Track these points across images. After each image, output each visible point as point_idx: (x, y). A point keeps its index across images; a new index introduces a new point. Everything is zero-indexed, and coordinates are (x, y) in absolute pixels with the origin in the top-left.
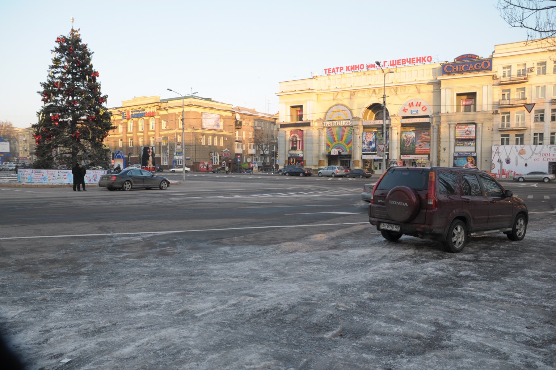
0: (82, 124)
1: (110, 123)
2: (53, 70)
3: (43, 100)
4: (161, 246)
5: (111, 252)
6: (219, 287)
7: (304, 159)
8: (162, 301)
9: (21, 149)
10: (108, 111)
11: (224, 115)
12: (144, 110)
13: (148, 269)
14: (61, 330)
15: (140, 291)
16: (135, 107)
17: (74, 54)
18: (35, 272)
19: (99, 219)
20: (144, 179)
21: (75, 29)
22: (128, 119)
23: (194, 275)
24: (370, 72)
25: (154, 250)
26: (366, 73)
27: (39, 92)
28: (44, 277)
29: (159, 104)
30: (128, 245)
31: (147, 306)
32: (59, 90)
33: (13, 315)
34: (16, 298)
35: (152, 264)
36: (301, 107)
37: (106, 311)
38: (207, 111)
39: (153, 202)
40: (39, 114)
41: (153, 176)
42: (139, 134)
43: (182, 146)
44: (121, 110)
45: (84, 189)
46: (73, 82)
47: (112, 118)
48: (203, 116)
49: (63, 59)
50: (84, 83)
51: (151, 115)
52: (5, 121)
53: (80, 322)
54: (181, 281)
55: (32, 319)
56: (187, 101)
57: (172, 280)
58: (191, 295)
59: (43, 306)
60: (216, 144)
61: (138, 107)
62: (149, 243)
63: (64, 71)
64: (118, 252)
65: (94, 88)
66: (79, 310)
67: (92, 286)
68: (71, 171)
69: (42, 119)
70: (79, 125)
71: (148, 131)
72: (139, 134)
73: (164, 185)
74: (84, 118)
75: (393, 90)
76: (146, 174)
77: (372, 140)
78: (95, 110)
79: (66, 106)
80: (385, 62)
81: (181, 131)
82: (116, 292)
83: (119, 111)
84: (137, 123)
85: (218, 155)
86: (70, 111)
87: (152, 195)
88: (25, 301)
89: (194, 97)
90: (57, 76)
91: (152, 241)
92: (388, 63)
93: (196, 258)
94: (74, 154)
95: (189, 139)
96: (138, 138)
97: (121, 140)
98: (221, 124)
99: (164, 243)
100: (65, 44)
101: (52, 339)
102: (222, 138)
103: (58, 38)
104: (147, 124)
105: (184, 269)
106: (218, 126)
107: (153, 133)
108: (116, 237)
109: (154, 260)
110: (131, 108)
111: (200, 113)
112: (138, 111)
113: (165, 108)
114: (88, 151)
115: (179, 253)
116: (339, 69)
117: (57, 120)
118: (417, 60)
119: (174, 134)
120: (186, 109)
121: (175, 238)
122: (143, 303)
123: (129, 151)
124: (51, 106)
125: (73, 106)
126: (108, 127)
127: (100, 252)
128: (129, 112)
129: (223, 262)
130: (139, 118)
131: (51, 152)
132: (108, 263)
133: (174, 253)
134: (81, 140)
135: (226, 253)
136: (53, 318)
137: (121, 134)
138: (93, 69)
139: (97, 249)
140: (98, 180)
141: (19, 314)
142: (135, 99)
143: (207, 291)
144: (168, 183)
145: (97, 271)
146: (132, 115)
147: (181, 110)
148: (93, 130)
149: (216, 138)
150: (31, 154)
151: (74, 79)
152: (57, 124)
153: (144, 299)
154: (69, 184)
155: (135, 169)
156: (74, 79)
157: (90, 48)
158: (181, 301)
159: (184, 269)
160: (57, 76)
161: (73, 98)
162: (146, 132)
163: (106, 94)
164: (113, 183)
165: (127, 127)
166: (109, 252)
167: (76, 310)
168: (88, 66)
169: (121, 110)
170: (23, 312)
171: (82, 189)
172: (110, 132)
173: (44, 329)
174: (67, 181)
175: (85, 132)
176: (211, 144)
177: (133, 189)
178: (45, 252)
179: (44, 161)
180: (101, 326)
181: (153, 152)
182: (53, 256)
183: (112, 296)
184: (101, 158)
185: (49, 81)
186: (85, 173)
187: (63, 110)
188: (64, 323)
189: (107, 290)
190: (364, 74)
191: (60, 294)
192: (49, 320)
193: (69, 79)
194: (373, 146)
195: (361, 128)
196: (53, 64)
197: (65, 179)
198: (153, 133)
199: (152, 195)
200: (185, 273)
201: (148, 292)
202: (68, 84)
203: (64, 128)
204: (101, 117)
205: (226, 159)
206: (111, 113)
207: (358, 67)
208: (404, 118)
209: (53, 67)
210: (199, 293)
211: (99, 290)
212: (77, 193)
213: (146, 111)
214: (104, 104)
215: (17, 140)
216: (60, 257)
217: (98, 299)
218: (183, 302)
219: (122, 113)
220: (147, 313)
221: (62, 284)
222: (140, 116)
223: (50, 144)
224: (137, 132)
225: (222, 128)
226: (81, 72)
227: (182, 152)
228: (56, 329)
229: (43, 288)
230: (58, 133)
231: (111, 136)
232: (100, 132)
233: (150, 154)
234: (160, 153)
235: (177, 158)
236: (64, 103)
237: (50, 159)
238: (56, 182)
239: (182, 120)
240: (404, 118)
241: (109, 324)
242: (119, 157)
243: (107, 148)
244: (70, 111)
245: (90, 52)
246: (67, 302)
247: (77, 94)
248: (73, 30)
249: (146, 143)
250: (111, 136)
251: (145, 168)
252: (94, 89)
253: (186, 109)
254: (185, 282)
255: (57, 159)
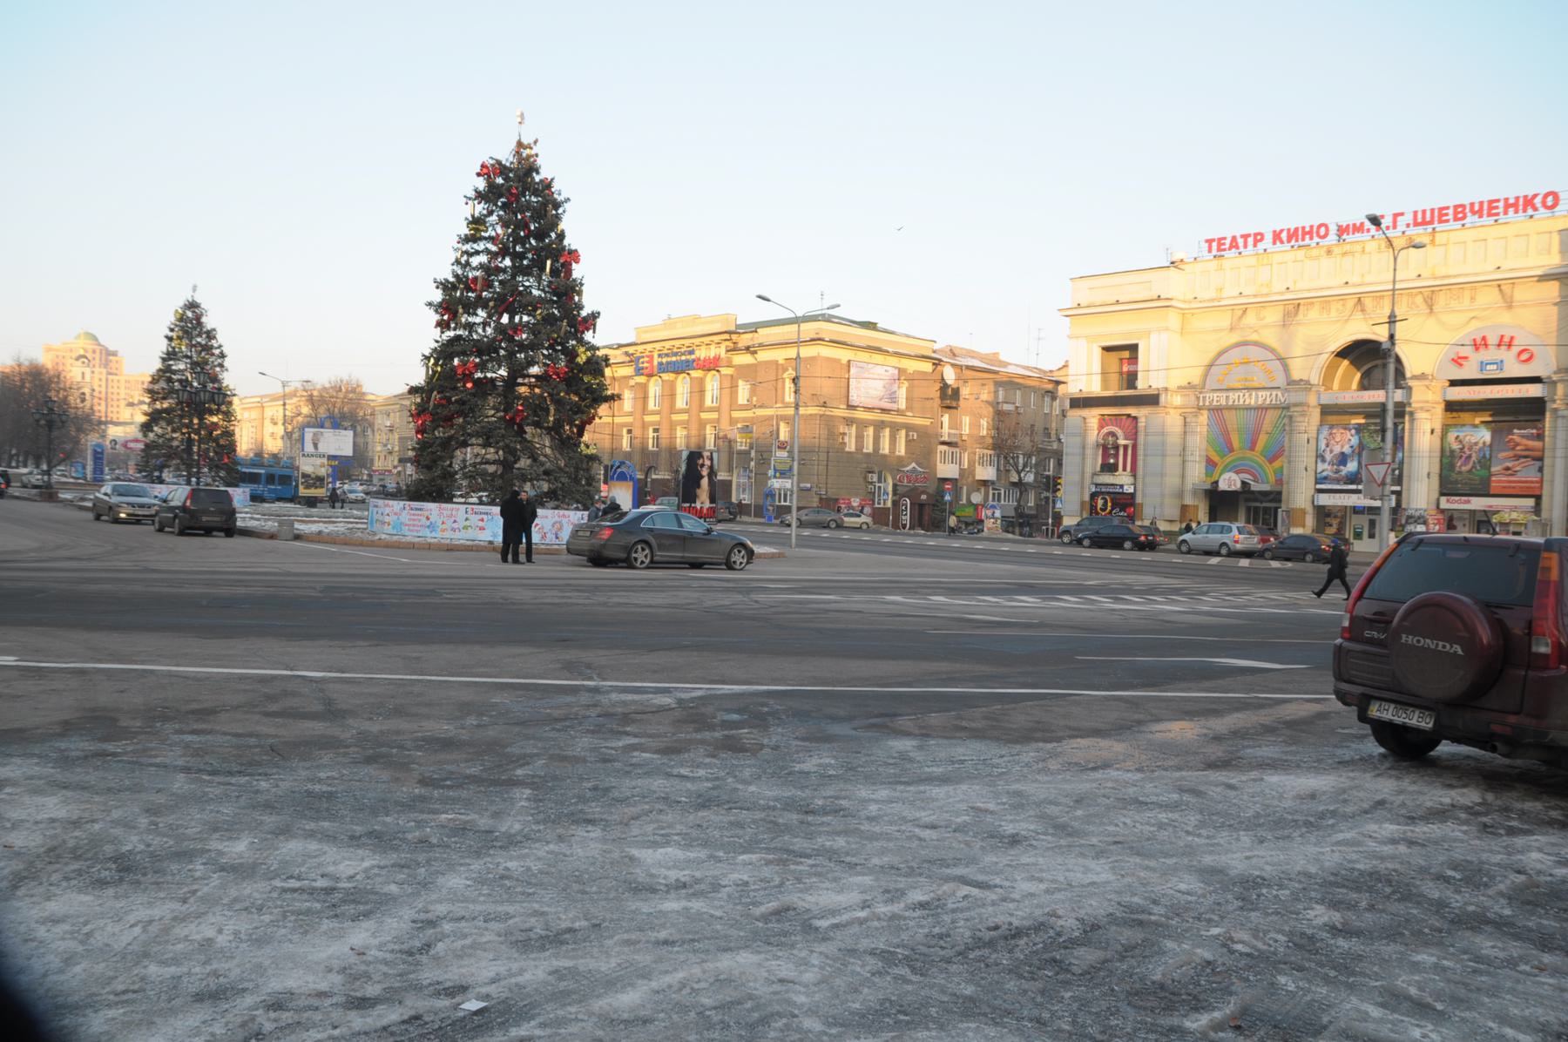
0: (531, 386)
1: (602, 387)
2: (467, 247)
3: (439, 324)
4: (726, 725)
5: (593, 732)
6: (883, 852)
7: (1139, 500)
8: (725, 875)
9: (379, 448)
10: (599, 353)
11: (911, 370)
12: (691, 352)
13: (689, 785)
14: (463, 924)
15: (667, 844)
16: (668, 345)
17: (519, 200)
18: (405, 766)
19: (564, 642)
20: (685, 539)
21: (525, 142)
22: (650, 376)
23: (813, 812)
24: (1347, 248)
25: (707, 735)
26: (1336, 250)
27: (430, 304)
28: (424, 782)
29: (734, 337)
30: (639, 717)
31: (685, 886)
32: (479, 297)
33: (351, 872)
34: (359, 829)
35: (701, 771)
36: (1133, 348)
37: (576, 887)
38: (864, 356)
39: (708, 603)
40: (428, 358)
41: (709, 531)
42: (675, 417)
43: (791, 452)
44: (631, 350)
45: (529, 560)
46: (514, 276)
47: (608, 372)
48: (853, 371)
49: (494, 218)
50: (539, 280)
51: (712, 365)
52: (345, 378)
53: (511, 909)
54: (776, 824)
55: (393, 888)
56: (809, 329)
57: (754, 821)
58: (804, 866)
59: (421, 858)
60: (885, 448)
61: (677, 343)
62: (695, 716)
63: (494, 248)
64: (612, 731)
65: (566, 291)
66: (508, 878)
67: (542, 816)
68: (497, 510)
69: (434, 372)
70: (523, 390)
71: (702, 408)
72: (675, 417)
73: (738, 558)
74: (535, 370)
75: (1419, 300)
76: (692, 525)
77: (1347, 449)
78: (565, 351)
79: (494, 339)
80: (1396, 216)
81: (791, 411)
82: (604, 840)
83: (627, 354)
84: (701, 382)
85: (890, 481)
86: (502, 352)
87: (706, 583)
88: (380, 840)
89: (828, 319)
90: (475, 261)
91: (703, 710)
92: (1409, 218)
93: (819, 765)
94: (507, 465)
95: (812, 434)
96: (672, 426)
97: (630, 432)
98: (902, 393)
99: (735, 717)
100: (500, 181)
101: (440, 945)
102: (903, 433)
103: (483, 166)
104: (699, 390)
105: (788, 792)
106: (893, 398)
107: (714, 415)
108: (608, 692)
109: (708, 760)
110: (658, 346)
111: (844, 361)
112: (676, 354)
113: (747, 348)
114: (542, 458)
115: (776, 748)
116: (1250, 240)
117: (468, 376)
118: (1507, 206)
119: (770, 418)
120: (806, 352)
121: (766, 705)
122: (673, 875)
123: (649, 461)
124: (458, 338)
125: (511, 340)
126: (598, 397)
127: (564, 729)
128: (651, 357)
129: (894, 782)
130: (678, 373)
131: (452, 457)
132: (584, 760)
133: (762, 746)
134: (528, 429)
135: (904, 757)
136: (444, 891)
137: (630, 414)
138: (566, 242)
139: (557, 720)
140: (565, 535)
141: (366, 871)
142: (669, 322)
143: (848, 859)
144: (751, 553)
145: (555, 778)
146: (660, 364)
147: (791, 352)
148: (559, 403)
149: (887, 432)
150: (401, 461)
151: (518, 270)
152: (469, 385)
153: (677, 865)
154: (491, 543)
155: (660, 511)
156: (518, 270)
157: (561, 189)
158: (777, 880)
159: (788, 792)
160: (475, 261)
161: (511, 318)
162: (694, 412)
163: (596, 309)
164: (604, 546)
165: (645, 398)
166: (588, 731)
167: (502, 877)
168: (553, 235)
169: (631, 350)
170: (373, 867)
171: (522, 558)
172: (603, 409)
173: (423, 916)
174: (485, 536)
175: (537, 409)
176: (870, 450)
177: (654, 564)
178: (428, 717)
179: (433, 480)
180: (564, 925)
181: (711, 467)
182: (445, 728)
183: (594, 849)
184: (575, 481)
185: (456, 276)
186: (534, 515)
187: (486, 350)
188: (471, 906)
189: (580, 832)
190: (1329, 252)
191: (462, 830)
192: (435, 897)
193: (504, 270)
194: (1352, 466)
195: (1316, 415)
196: (467, 231)
197: (482, 529)
198: (714, 415)
199: (706, 583)
200: (790, 805)
201: (688, 846)
202: (501, 282)
203: (485, 395)
204: (581, 369)
205: (913, 493)
206: (606, 359)
207: (1309, 233)
208: (1453, 383)
209: (467, 239)
210: (826, 863)
211: (560, 831)
212: (511, 569)
213: (697, 354)
214: (588, 336)
215: (371, 425)
216: (465, 735)
217: (557, 854)
218: (782, 884)
219: (633, 360)
220: (684, 903)
221: (468, 804)
222: (680, 368)
223: (450, 438)
224: (673, 410)
225: (902, 405)
226: (536, 250)
227: (791, 469)
228: (452, 920)
229: (422, 812)
230: (472, 410)
231: (605, 420)
232: (577, 410)
233: (705, 472)
234: (730, 470)
235: (776, 484)
236: (489, 331)
237: (449, 475)
238: (461, 537)
239: (795, 380)
240: (1453, 383)
241: (584, 923)
242: (623, 477)
243: (591, 451)
244: (502, 352)
245: (560, 198)
246: (478, 854)
247: (523, 309)
248: (520, 144)
249: (694, 441)
250: (605, 420)
251: (689, 510)
252: (566, 294)
253: (806, 352)
254: (787, 829)
255: (465, 476)
